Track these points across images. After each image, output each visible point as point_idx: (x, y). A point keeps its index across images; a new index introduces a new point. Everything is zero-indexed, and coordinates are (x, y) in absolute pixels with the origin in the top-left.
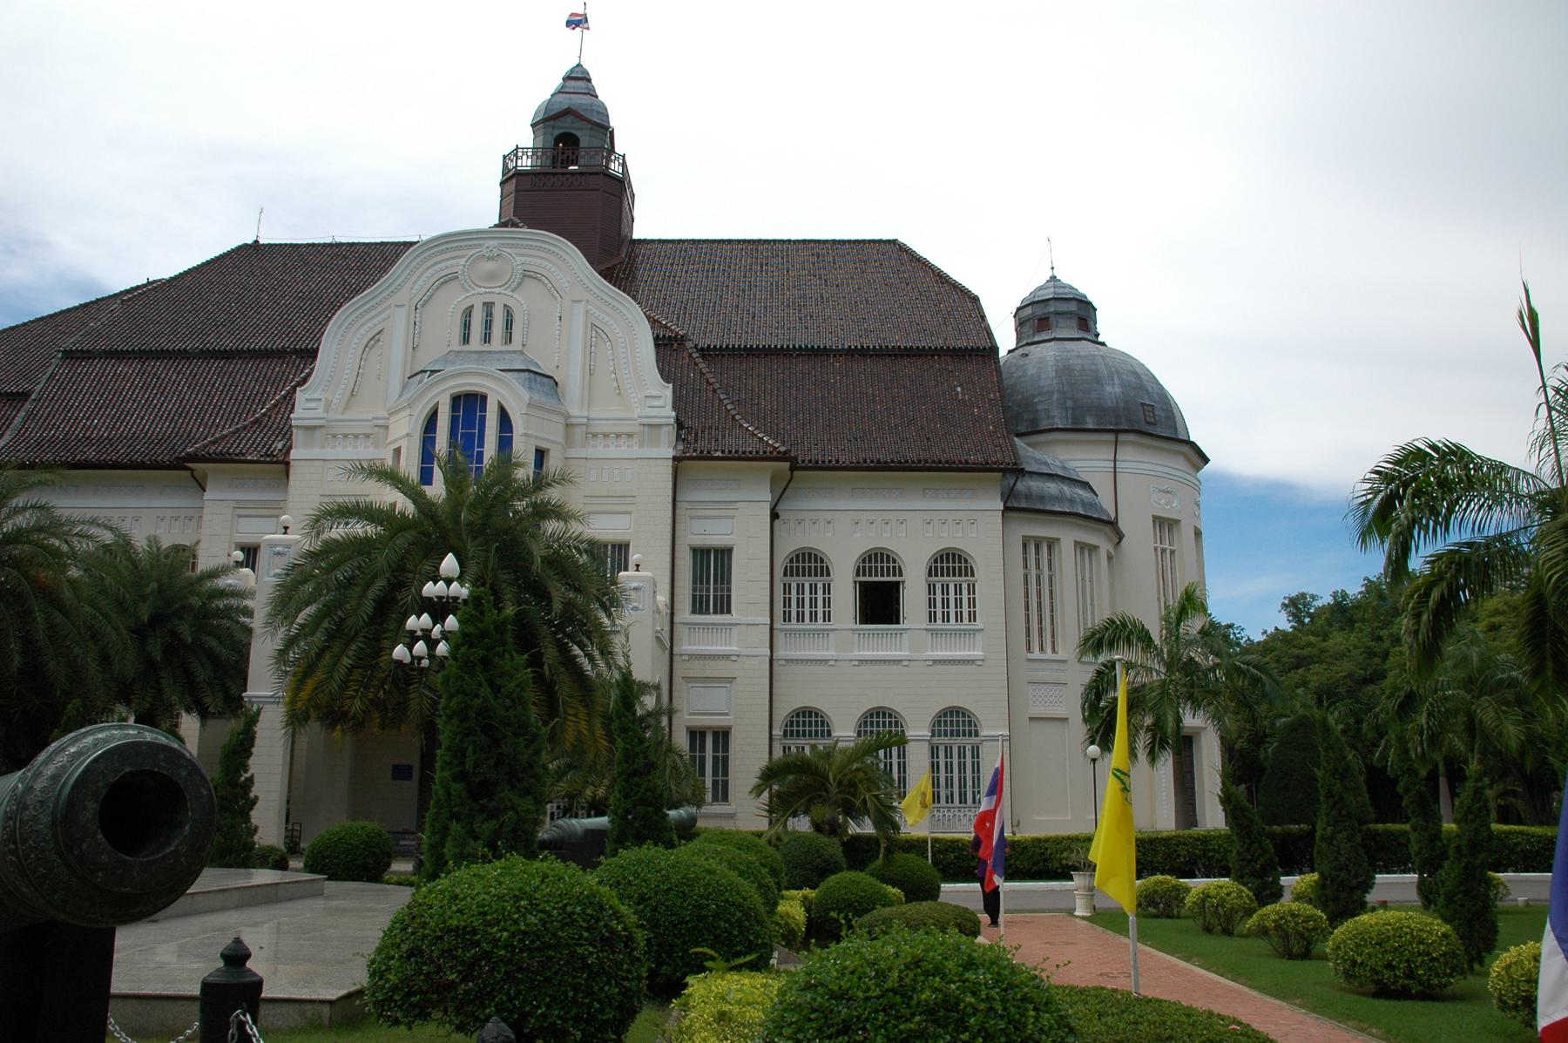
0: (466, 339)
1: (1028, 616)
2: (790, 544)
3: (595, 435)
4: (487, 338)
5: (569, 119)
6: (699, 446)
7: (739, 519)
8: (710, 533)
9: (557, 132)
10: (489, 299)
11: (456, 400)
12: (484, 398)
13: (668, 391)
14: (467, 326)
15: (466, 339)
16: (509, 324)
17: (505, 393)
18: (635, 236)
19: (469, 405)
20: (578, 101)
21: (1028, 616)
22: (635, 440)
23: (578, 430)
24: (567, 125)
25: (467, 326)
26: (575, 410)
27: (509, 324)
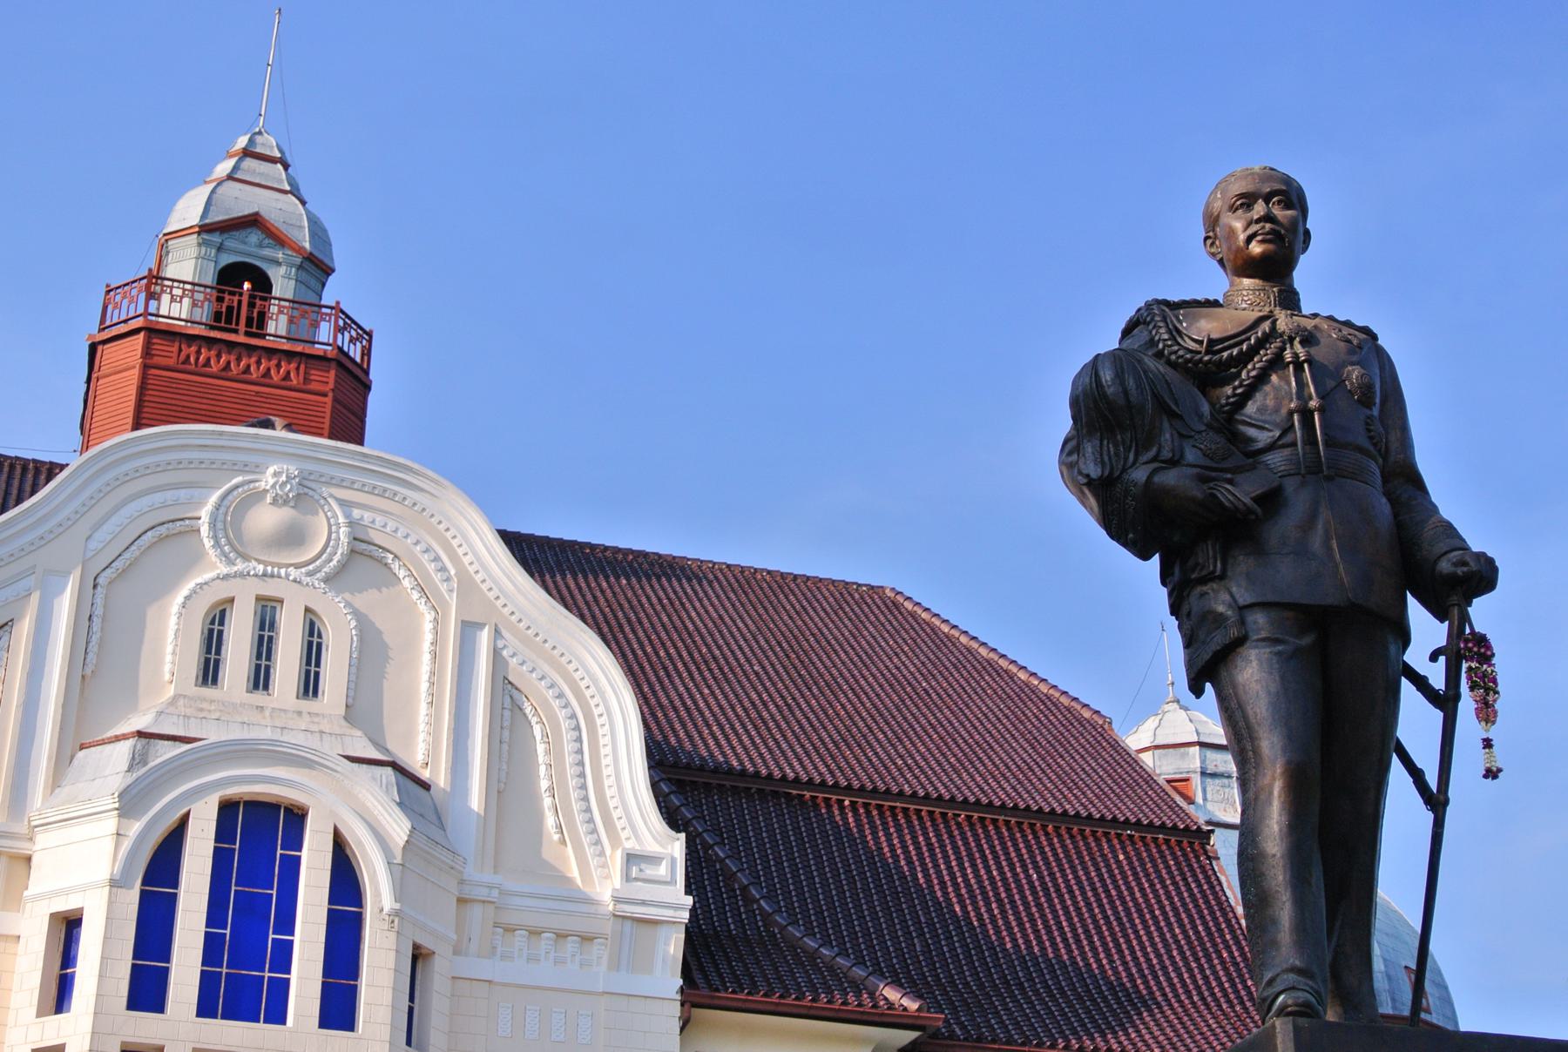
0: (210, 673)
1: (644, 903)
3: (510, 930)
4: (261, 679)
5: (254, 237)
9: (227, 259)
10: (270, 589)
11: (227, 809)
12: (296, 817)
13: (676, 846)
14: (213, 642)
15: (210, 673)
16: (313, 652)
17: (350, 810)
18: (1406, 658)
19: (259, 835)
21: (644, 903)
22: (598, 951)
23: (477, 912)
24: (246, 248)
25: (213, 642)
26: (479, 874)
27: (313, 652)
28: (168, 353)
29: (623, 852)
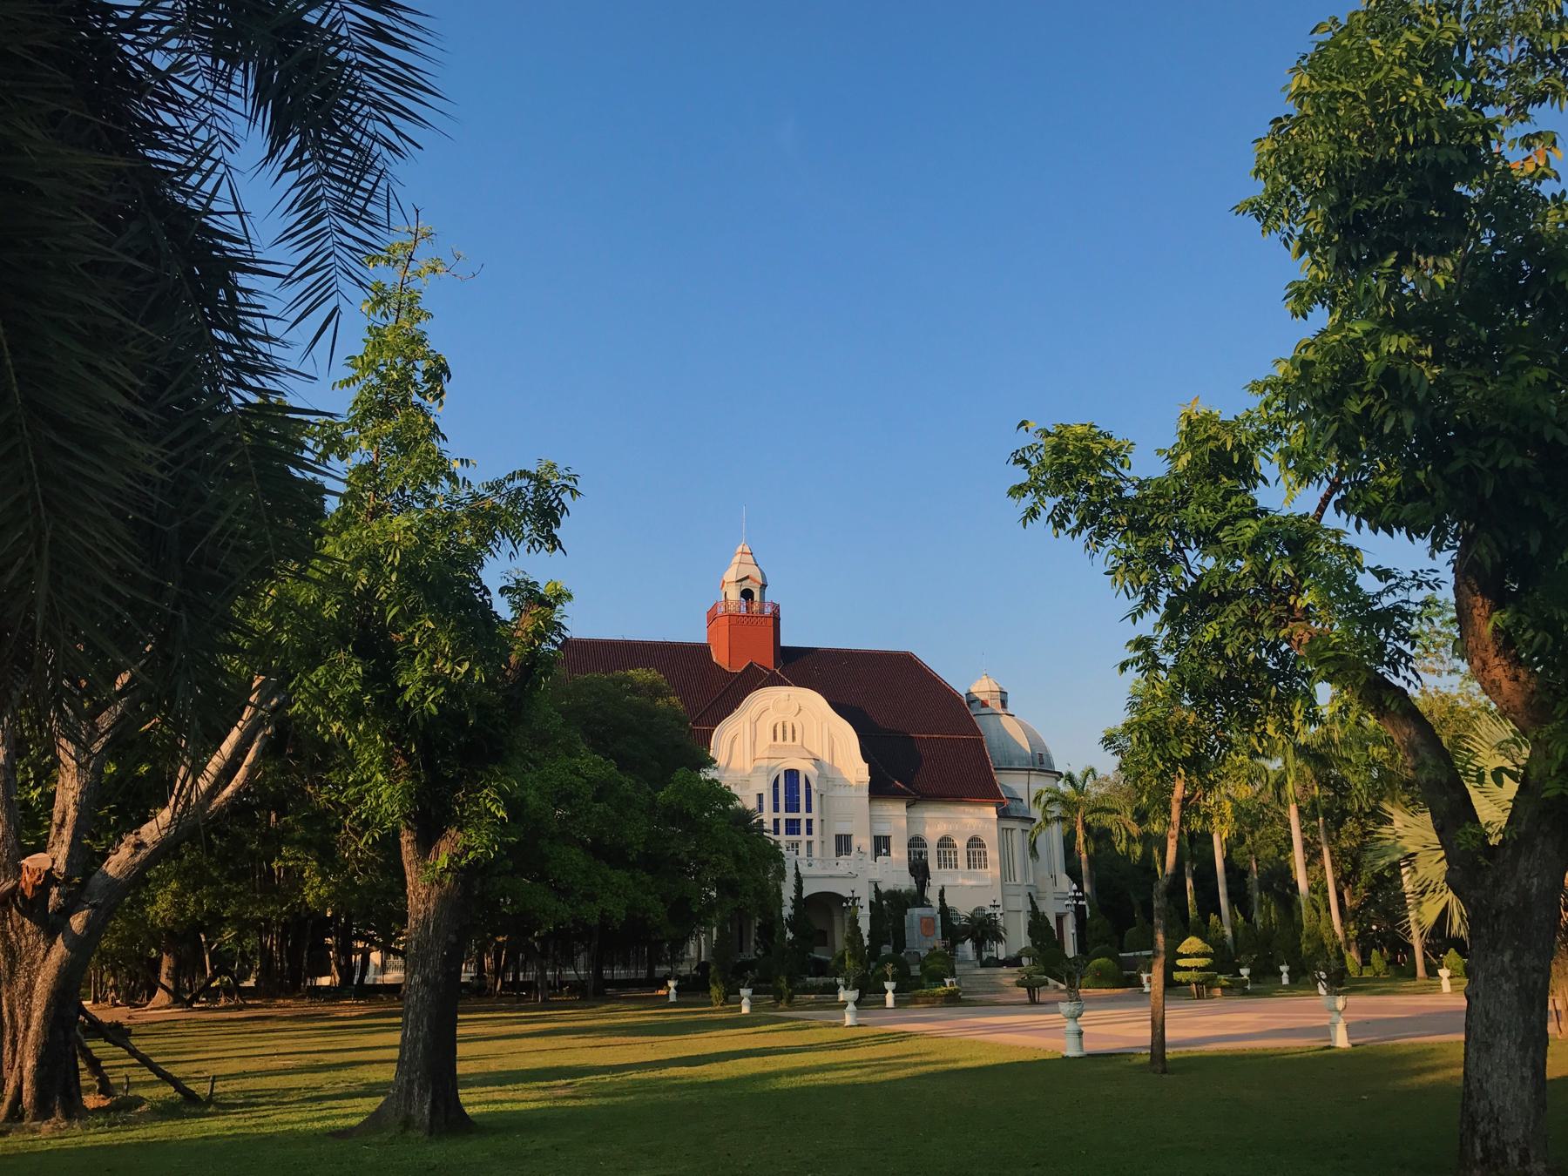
2: (913, 834)
6: (879, 789)
7: (895, 817)
8: (883, 830)
17: (805, 767)
19: (792, 775)
20: (754, 572)
24: (747, 584)
28: (734, 620)
29: (856, 770)
